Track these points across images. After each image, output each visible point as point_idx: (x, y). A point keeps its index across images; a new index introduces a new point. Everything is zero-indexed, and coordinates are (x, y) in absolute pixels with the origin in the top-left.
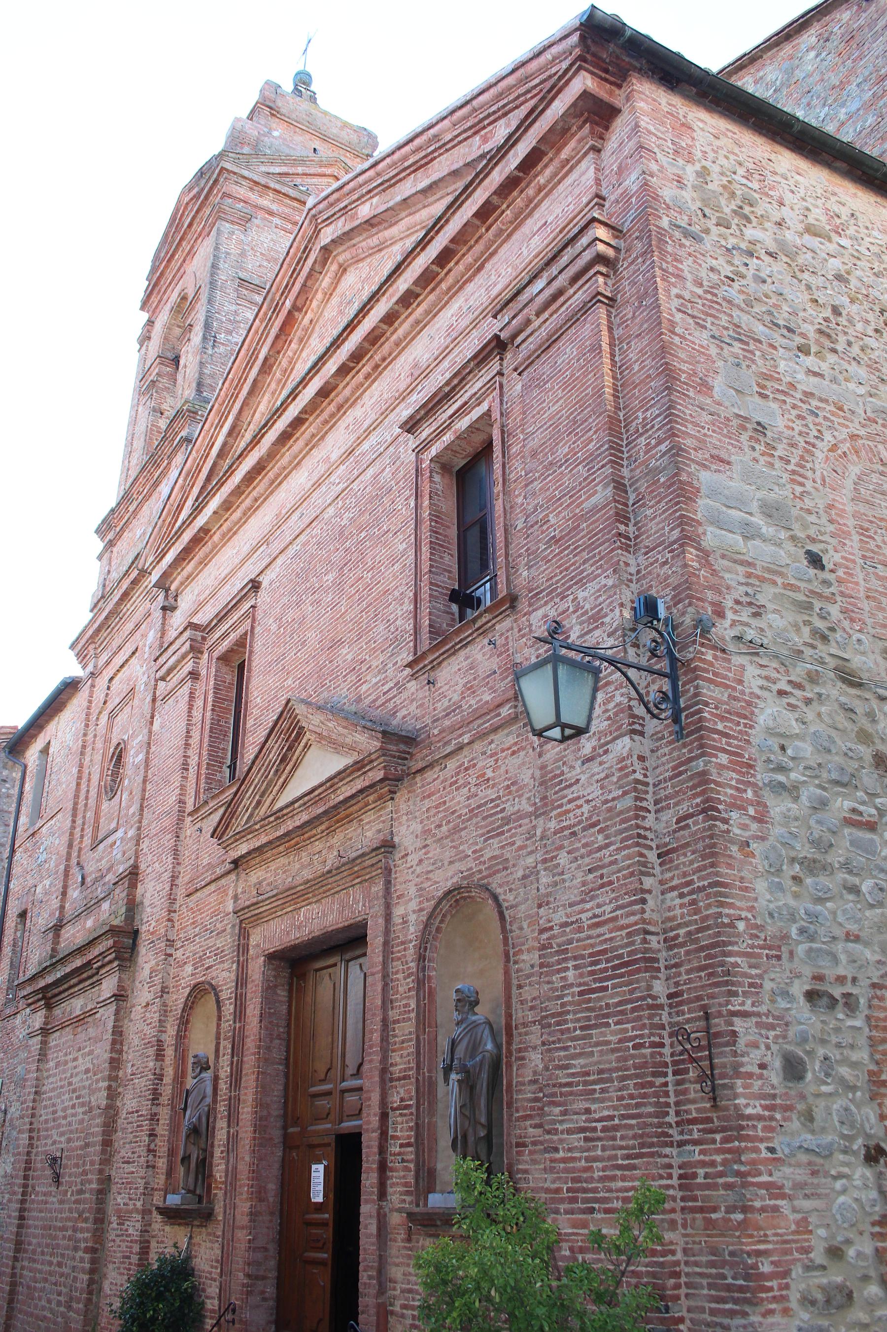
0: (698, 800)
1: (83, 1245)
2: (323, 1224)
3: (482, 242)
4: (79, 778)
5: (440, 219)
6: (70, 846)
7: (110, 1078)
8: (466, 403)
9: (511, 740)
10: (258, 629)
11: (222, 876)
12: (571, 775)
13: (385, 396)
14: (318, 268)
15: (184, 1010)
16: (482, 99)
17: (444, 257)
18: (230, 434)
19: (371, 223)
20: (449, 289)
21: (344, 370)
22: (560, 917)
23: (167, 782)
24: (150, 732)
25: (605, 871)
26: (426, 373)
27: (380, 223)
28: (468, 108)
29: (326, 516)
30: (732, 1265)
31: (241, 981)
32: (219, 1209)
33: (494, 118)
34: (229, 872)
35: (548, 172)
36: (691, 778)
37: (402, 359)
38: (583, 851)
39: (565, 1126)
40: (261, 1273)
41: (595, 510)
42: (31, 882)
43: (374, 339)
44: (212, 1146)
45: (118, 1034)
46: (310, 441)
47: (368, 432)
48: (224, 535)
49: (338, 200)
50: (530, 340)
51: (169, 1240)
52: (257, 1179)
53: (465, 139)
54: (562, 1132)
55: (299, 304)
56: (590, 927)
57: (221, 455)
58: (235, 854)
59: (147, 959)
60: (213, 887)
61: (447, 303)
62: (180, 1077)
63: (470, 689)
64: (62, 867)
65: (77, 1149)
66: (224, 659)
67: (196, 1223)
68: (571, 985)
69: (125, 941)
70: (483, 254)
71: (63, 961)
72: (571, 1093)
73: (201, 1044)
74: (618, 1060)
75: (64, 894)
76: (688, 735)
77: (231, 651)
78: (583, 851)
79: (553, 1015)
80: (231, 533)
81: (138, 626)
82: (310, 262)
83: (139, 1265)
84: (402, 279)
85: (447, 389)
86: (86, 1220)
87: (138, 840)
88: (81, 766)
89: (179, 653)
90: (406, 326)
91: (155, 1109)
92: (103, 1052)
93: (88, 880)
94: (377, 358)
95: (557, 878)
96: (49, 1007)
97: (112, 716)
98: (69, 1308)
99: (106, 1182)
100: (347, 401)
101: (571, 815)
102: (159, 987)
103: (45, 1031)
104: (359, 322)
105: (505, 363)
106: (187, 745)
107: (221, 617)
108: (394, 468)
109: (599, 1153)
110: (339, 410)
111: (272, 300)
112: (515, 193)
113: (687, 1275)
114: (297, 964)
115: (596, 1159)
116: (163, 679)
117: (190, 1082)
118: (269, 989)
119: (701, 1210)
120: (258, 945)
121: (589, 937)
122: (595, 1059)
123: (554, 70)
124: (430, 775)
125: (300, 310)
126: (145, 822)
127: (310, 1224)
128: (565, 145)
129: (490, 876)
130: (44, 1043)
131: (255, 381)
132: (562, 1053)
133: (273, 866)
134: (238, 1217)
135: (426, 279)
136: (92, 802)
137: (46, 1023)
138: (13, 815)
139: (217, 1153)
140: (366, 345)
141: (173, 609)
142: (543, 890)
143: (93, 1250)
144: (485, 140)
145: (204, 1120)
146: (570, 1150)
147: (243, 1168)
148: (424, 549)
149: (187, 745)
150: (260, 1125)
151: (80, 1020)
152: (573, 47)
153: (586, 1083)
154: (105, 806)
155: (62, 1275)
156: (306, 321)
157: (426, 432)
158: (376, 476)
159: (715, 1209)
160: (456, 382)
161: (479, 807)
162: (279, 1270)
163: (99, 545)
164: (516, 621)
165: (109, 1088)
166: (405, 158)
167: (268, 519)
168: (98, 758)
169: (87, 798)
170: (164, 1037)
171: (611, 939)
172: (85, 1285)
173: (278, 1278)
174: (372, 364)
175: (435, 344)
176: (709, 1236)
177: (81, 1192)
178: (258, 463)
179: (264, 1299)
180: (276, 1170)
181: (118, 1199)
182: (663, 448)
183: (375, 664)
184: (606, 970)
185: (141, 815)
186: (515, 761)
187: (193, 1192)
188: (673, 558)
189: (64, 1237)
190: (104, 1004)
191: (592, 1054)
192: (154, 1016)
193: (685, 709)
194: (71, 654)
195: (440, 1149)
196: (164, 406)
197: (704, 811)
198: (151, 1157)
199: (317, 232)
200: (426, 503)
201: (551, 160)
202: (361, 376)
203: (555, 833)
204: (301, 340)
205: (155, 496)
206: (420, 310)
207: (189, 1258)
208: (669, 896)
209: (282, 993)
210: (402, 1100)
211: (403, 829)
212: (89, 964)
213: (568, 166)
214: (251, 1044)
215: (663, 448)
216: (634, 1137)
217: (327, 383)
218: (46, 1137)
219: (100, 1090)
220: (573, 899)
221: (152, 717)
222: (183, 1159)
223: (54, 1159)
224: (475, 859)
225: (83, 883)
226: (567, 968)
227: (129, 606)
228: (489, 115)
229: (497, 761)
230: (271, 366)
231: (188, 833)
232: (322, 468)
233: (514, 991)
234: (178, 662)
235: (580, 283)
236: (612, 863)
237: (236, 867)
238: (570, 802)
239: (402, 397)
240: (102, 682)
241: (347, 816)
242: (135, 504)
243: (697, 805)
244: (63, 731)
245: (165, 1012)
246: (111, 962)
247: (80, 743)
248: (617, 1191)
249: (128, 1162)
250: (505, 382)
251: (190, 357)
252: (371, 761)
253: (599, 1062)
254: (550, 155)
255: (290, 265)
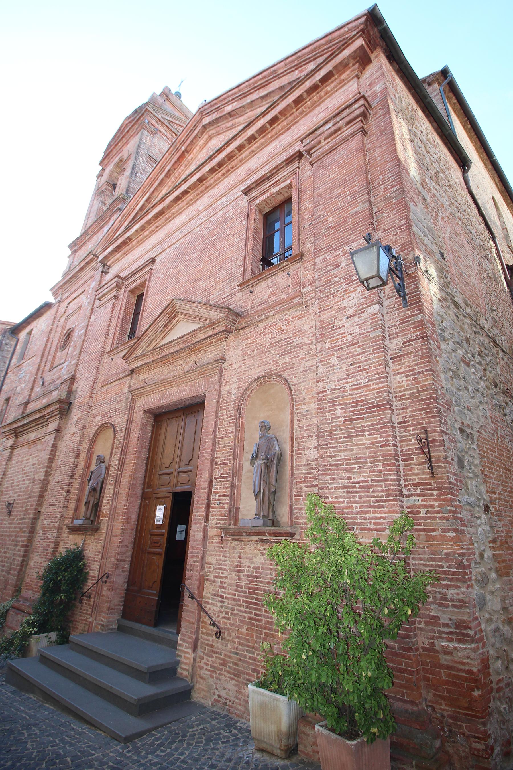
0: (418, 333)
1: (21, 544)
2: (162, 535)
3: (293, 116)
4: (47, 342)
5: (275, 102)
6: (38, 370)
7: (48, 467)
8: (279, 180)
9: (298, 313)
10: (152, 278)
11: (123, 378)
12: (338, 323)
13: (231, 183)
14: (199, 135)
15: (94, 436)
16: (304, 51)
17: (274, 121)
18: (147, 201)
19: (230, 114)
20: (272, 137)
21: (213, 170)
22: (332, 385)
23: (97, 340)
24: (89, 321)
25: (361, 364)
26: (256, 171)
27: (235, 115)
28: (296, 56)
29: (194, 232)
30: (447, 560)
31: (129, 422)
32: (104, 527)
33: (307, 61)
34: (127, 376)
35: (333, 85)
36: (413, 324)
37: (242, 168)
38: (347, 356)
39: (333, 486)
40: (124, 558)
41: (357, 213)
42: (14, 385)
43: (230, 157)
44: (103, 497)
45: (55, 447)
46: (189, 202)
47: (221, 197)
48: (138, 242)
49: (216, 104)
50: (319, 151)
51: (71, 542)
52: (127, 513)
53: (290, 72)
54: (331, 489)
55: (188, 149)
56: (351, 390)
57: (141, 209)
58: (133, 366)
59: (76, 414)
60: (117, 382)
61: (269, 144)
62: (88, 465)
63: (274, 294)
64: (33, 378)
65: (23, 499)
66: (132, 291)
67: (89, 533)
68: (339, 417)
69: (65, 407)
70: (292, 122)
71: (28, 415)
72: (338, 469)
73: (102, 449)
74: (371, 452)
75: (32, 389)
76: (410, 305)
77: (136, 288)
78: (347, 356)
79: (326, 432)
80: (142, 241)
81: (86, 282)
82: (196, 132)
83: (52, 554)
84: (249, 130)
85: (269, 175)
86: (24, 532)
87: (77, 365)
88: (49, 337)
89: (110, 288)
90: (247, 152)
91: (71, 480)
92: (45, 455)
93: (46, 384)
94: (229, 167)
95: (330, 369)
96: (16, 437)
97: (67, 318)
98: (9, 573)
99: (37, 515)
100: (210, 186)
101: (340, 340)
102: (81, 426)
103: (13, 447)
104: (225, 149)
105: (300, 164)
106: (109, 325)
107: (133, 274)
108: (234, 210)
109: (357, 499)
110: (206, 189)
111: (176, 146)
112: (314, 94)
113: (414, 565)
114: (159, 417)
115: (354, 502)
116: (99, 299)
117: (93, 468)
118: (144, 426)
119: (424, 530)
120: (140, 406)
121: (351, 395)
122: (355, 452)
123: (347, 36)
124: (247, 330)
125: (188, 152)
126: (81, 358)
127: (152, 535)
128: (344, 72)
129: (283, 371)
130: (11, 453)
131: (162, 179)
132: (332, 450)
133: (153, 372)
134: (114, 531)
135: (262, 131)
136: (52, 352)
137: (14, 444)
138: (9, 359)
139: (105, 500)
140: (226, 159)
141: (106, 273)
142: (320, 374)
143: (27, 546)
144: (301, 71)
145: (99, 485)
146: (336, 497)
147: (120, 508)
148: (250, 240)
149: (109, 325)
150: (132, 487)
151: (33, 442)
152: (361, 24)
153: (347, 464)
154: (59, 354)
155: (6, 557)
156: (190, 158)
157: (254, 194)
158: (223, 214)
159: (434, 530)
160: (274, 171)
161: (277, 342)
162: (132, 557)
163: (70, 252)
164: (302, 264)
165: (46, 471)
166: (256, 82)
167: (162, 235)
168: (58, 335)
169: (50, 351)
170: (81, 448)
171: (366, 395)
172: (19, 563)
173: (131, 561)
174: (227, 169)
175: (262, 160)
176: (429, 544)
177: (23, 519)
178: (162, 210)
179: (123, 571)
180: (136, 509)
181: (44, 522)
182: (395, 188)
183: (218, 287)
184: (361, 409)
185: (80, 355)
186: (300, 322)
187: (88, 519)
188: (401, 232)
189: (10, 540)
190: (49, 434)
191: (353, 450)
192: (77, 438)
193: (408, 294)
194: (50, 294)
195: (242, 498)
196: (106, 202)
197: (422, 337)
198: (66, 503)
199: (201, 119)
200: (252, 222)
201: (336, 79)
202: (220, 174)
203: (329, 349)
204: (186, 166)
205: (101, 232)
206: (256, 146)
207: (82, 550)
208: (398, 376)
209: (149, 428)
210: (222, 474)
211: (231, 354)
212: (43, 416)
213: (344, 83)
214: (131, 450)
215: (395, 188)
216: (382, 491)
217: (204, 175)
218: (6, 495)
219: (41, 472)
220: (340, 378)
221: (91, 315)
222: (86, 503)
223: (10, 504)
224: (273, 365)
225: (43, 385)
226: (336, 409)
227: (83, 274)
228: (306, 60)
229: (289, 322)
230: (170, 175)
231: (105, 361)
232: (194, 213)
233: (295, 422)
234: (109, 291)
235: (350, 125)
236: (365, 361)
237: (131, 373)
238: (338, 335)
239: (241, 182)
240: (64, 305)
241: (199, 348)
242: (89, 236)
243: (417, 335)
244: (41, 325)
245: (83, 437)
246: (56, 415)
247: (50, 328)
248: (370, 519)
249: (53, 505)
250: (300, 171)
251: (123, 181)
252: (219, 322)
253: (358, 454)
254: (336, 77)
255: (186, 132)
